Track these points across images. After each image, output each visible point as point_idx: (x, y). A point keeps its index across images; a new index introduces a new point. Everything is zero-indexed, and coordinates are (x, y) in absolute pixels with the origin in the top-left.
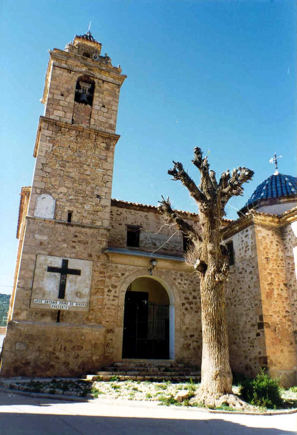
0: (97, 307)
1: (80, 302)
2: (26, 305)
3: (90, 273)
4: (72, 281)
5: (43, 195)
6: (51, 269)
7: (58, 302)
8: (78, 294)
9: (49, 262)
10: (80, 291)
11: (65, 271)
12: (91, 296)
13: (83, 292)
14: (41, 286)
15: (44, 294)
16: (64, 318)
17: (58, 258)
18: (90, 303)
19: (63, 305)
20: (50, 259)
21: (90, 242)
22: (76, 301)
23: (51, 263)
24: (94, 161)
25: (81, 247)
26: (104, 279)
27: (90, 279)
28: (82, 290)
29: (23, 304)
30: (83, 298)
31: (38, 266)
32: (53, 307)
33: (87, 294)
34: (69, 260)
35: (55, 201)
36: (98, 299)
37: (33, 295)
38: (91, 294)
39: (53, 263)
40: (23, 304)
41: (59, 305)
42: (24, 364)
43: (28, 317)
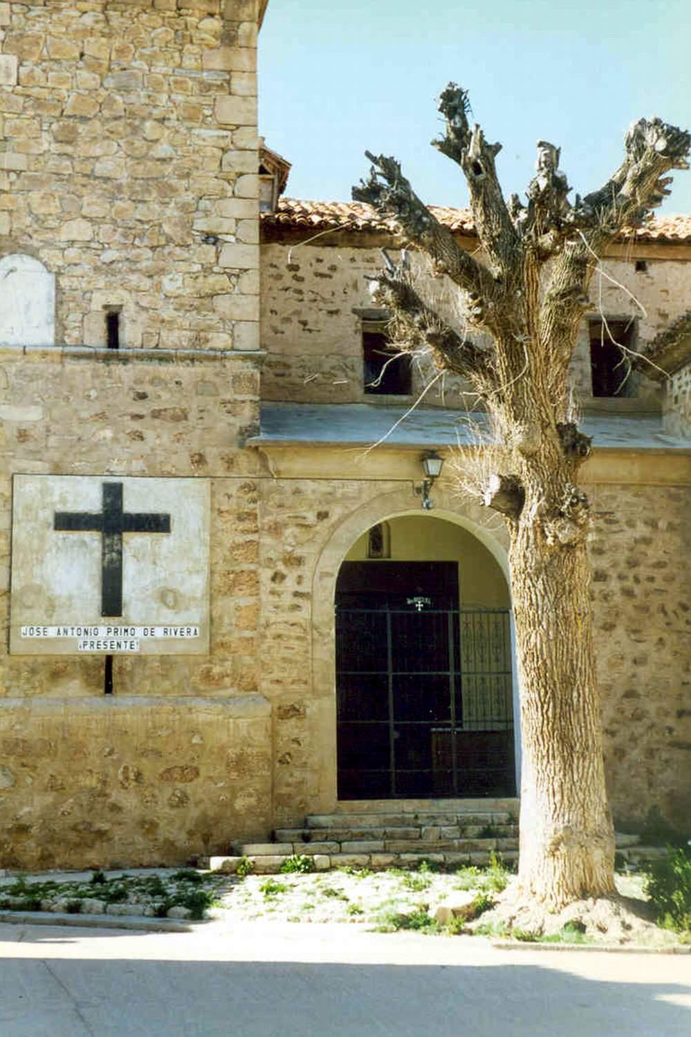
4: (144, 556)
6: (67, 522)
8: (167, 597)
9: (56, 498)
11: (113, 521)
12: (212, 600)
14: (38, 582)
16: (127, 679)
19: (121, 637)
20: (59, 485)
21: (193, 415)
23: (63, 501)
31: (20, 516)
32: (87, 648)
33: (199, 595)
35: (52, 277)
36: (238, 609)
38: (212, 595)
39: (70, 498)
41: (104, 638)
42: (9, 831)
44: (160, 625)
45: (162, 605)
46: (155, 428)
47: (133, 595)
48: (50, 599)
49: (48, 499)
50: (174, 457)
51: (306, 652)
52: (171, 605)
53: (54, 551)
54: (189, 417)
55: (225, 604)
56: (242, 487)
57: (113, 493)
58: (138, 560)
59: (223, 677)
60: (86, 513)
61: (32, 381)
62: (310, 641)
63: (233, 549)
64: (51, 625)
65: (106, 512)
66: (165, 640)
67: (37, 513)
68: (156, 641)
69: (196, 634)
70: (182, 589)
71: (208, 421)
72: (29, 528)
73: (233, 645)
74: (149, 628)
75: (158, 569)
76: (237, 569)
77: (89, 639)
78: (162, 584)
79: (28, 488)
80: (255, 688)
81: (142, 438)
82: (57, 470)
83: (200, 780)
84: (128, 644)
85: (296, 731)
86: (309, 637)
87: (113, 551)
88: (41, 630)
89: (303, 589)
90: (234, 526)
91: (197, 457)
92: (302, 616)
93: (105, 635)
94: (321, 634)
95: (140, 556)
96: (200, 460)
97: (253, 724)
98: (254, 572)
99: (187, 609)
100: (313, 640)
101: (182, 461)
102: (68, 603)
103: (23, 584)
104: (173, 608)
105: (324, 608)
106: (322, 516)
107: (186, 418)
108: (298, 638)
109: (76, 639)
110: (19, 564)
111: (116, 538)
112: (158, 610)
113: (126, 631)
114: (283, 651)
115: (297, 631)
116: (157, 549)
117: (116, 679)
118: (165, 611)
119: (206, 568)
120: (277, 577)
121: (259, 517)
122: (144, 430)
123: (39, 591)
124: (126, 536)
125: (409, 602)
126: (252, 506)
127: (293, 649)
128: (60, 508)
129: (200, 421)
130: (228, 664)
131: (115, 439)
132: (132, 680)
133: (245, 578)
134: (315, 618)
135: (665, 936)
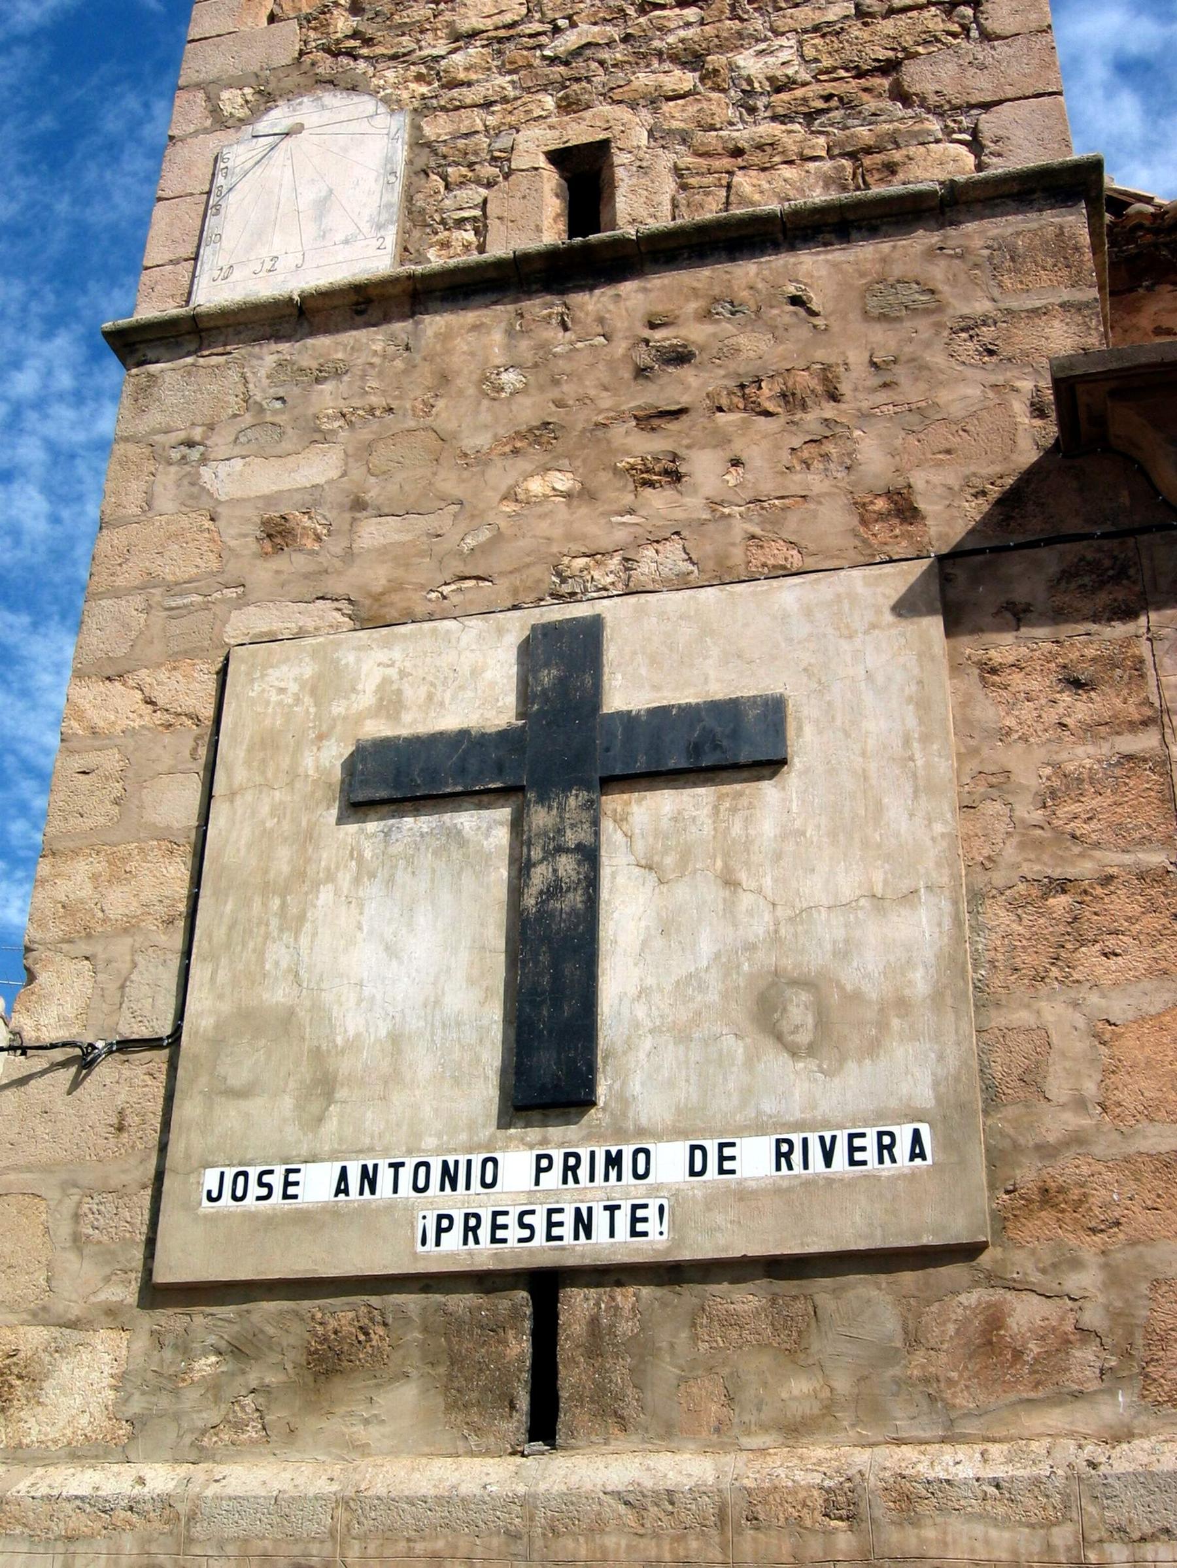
0: (1106, 1146)
1: (826, 1107)
2: (107, 1255)
3: (923, 705)
4: (685, 856)
5: (278, 117)
6: (397, 780)
7: (516, 1166)
8: (786, 1008)
9: (366, 699)
10: (815, 959)
11: (564, 752)
12: (985, 999)
13: (867, 972)
14: (279, 995)
15: (323, 1086)
16: (619, 1373)
17: (475, 623)
18: (999, 1087)
19: (593, 1192)
20: (372, 661)
21: (855, 381)
22: (769, 1106)
24: (784, 57)
25: (756, 455)
26: (1146, 742)
27: (923, 787)
28: (843, 953)
29: (78, 1242)
30: (873, 1048)
31: (241, 775)
32: (453, 1240)
33: (920, 983)
34: (614, 612)
36: (1104, 1032)
37: (187, 1109)
38: (976, 988)
39: (413, 694)
40: (78, 1242)
41: (525, 1192)
43: (136, 1406)
44: (759, 1129)
47: (641, 1012)
48: (317, 1055)
49: (338, 708)
52: (804, 1038)
56: (1067, 575)
60: (441, 733)
61: (318, 381)
63: (1049, 798)
64: (313, 1159)
66: (778, 1191)
68: (744, 1195)
69: (918, 1151)
70: (850, 977)
72: (265, 810)
73: (1098, 1196)
74: (712, 1148)
75: (746, 900)
76: (1084, 868)
77: (457, 1203)
78: (766, 959)
79: (270, 689)
82: (371, 616)
84: (623, 1219)
87: (561, 850)
88: (276, 1180)
90: (1051, 716)
93: (528, 1183)
95: (669, 861)
101: (832, 521)
102: (385, 1066)
103: (226, 1007)
104: (812, 1050)
109: (409, 1209)
110: (220, 934)
111: (573, 801)
112: (750, 1062)
113: (614, 1161)
117: (571, 1377)
118: (775, 1062)
124: (613, 802)
130: (1085, 1280)
135: (392, 337)
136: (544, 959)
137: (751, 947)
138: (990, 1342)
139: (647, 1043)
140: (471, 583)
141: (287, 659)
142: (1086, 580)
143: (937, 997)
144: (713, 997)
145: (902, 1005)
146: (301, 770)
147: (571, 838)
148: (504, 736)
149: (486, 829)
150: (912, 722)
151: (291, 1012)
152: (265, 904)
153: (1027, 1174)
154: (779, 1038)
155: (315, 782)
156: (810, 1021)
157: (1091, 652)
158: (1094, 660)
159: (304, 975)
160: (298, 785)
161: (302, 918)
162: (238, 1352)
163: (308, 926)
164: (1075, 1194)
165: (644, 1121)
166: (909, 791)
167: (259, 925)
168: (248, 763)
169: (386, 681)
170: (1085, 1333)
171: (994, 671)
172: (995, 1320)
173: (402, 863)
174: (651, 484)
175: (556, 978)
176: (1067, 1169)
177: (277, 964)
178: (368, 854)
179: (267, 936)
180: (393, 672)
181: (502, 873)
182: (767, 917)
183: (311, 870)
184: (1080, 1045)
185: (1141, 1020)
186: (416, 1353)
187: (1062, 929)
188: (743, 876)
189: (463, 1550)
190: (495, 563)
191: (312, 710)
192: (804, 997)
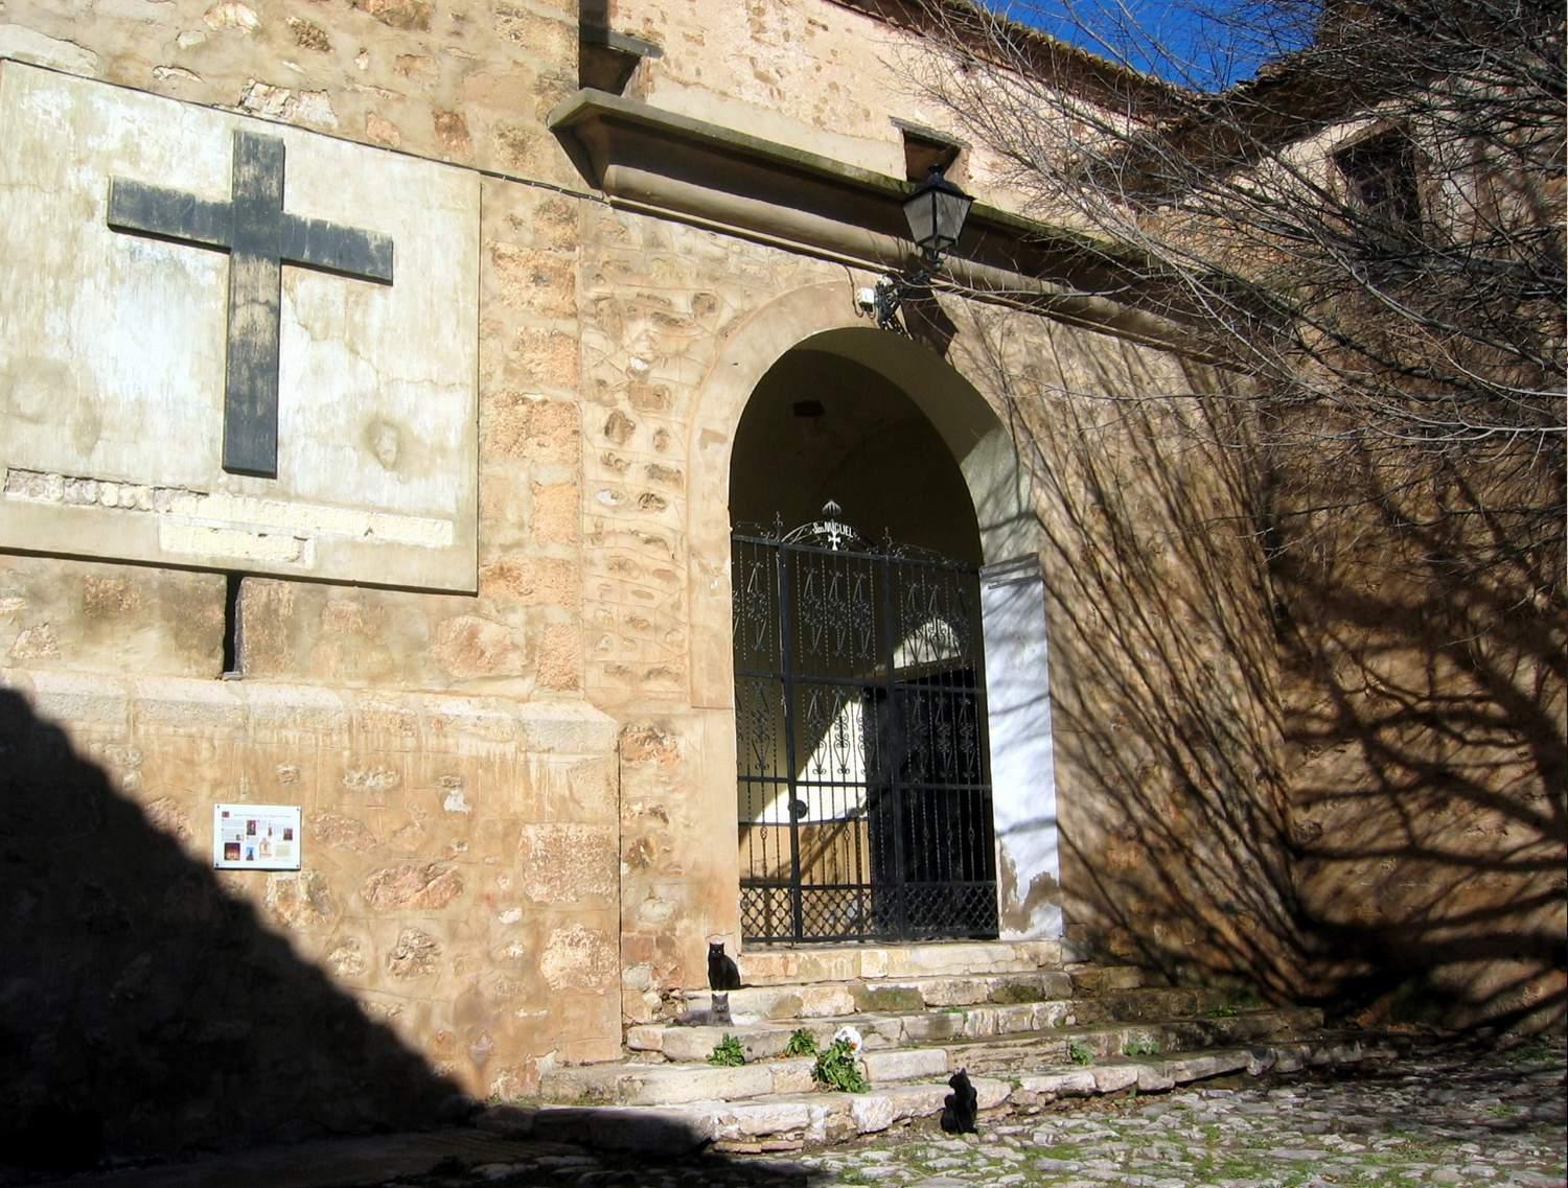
4: (327, 327)
6: (147, 215)
9: (113, 143)
10: (399, 414)
13: (424, 426)
14: (57, 353)
20: (119, 113)
23: (132, 153)
39: (150, 150)
41: (220, 526)
45: (370, 457)
46: (355, 32)
48: (87, 403)
50: (398, 107)
51: (676, 606)
53: (103, 278)
54: (433, 23)
55: (509, 472)
57: (261, 159)
58: (313, 339)
59: (505, 650)
62: (684, 584)
63: (520, 345)
65: (239, 201)
67: (61, 170)
70: (416, 428)
71: (471, 44)
73: (526, 577)
75: (362, 365)
80: (573, 684)
81: (325, 46)
83: (467, 901)
85: (659, 791)
86: (682, 575)
89: (669, 461)
90: (527, 295)
91: (445, 119)
92: (662, 522)
94: (704, 569)
95: (318, 326)
96: (452, 126)
97: (584, 765)
98: (569, 407)
99: (426, 473)
100: (690, 579)
104: (395, 466)
105: (703, 510)
106: (704, 304)
107: (424, 25)
108: (661, 574)
114: (632, 599)
115: (657, 558)
116: (358, 317)
117: (246, 636)
118: (373, 468)
119: (470, 380)
120: (619, 427)
121: (579, 280)
122: (330, 29)
123: (58, 376)
125: (818, 530)
126: (565, 254)
127: (650, 596)
128: (127, 173)
129: (454, 41)
131: (260, 33)
132: (291, 639)
133: (550, 417)
134: (693, 531)
136: (245, 373)
137: (363, 396)
138: (470, 643)
139: (302, 442)
140: (183, 73)
141: (50, 88)
142: (552, 215)
143: (461, 450)
144: (342, 421)
145: (442, 450)
146: (66, 184)
147: (262, 296)
148: (218, 210)
149: (206, 267)
150: (459, 277)
151: (66, 368)
152: (42, 281)
153: (493, 558)
154: (377, 455)
155: (77, 196)
156: (394, 449)
157: (550, 263)
158: (551, 269)
159: (74, 343)
160: (64, 194)
161: (71, 299)
162: (37, 596)
163: (76, 307)
164: (515, 573)
165: (300, 491)
166: (454, 322)
167: (39, 296)
168: (23, 164)
169: (128, 134)
170: (515, 647)
171: (500, 257)
172: (473, 634)
173: (143, 279)
174: (308, 44)
175: (252, 389)
176: (513, 559)
177: (54, 329)
178: (118, 265)
179: (45, 306)
180: (134, 128)
181: (219, 306)
182: (374, 378)
183: (77, 265)
184: (524, 493)
185: (553, 486)
186: (157, 612)
187: (521, 425)
188: (360, 348)
189: (207, 733)
190: (201, 64)
191: (72, 137)
192: (393, 434)
